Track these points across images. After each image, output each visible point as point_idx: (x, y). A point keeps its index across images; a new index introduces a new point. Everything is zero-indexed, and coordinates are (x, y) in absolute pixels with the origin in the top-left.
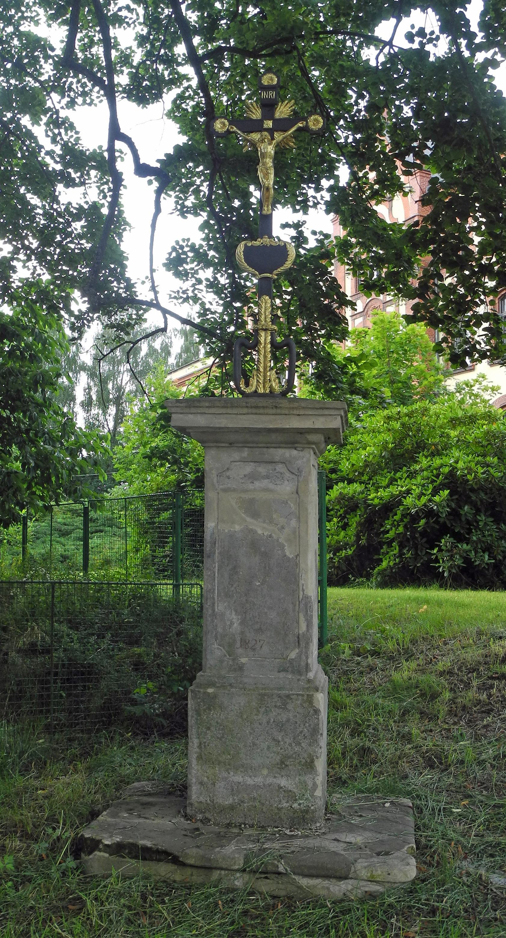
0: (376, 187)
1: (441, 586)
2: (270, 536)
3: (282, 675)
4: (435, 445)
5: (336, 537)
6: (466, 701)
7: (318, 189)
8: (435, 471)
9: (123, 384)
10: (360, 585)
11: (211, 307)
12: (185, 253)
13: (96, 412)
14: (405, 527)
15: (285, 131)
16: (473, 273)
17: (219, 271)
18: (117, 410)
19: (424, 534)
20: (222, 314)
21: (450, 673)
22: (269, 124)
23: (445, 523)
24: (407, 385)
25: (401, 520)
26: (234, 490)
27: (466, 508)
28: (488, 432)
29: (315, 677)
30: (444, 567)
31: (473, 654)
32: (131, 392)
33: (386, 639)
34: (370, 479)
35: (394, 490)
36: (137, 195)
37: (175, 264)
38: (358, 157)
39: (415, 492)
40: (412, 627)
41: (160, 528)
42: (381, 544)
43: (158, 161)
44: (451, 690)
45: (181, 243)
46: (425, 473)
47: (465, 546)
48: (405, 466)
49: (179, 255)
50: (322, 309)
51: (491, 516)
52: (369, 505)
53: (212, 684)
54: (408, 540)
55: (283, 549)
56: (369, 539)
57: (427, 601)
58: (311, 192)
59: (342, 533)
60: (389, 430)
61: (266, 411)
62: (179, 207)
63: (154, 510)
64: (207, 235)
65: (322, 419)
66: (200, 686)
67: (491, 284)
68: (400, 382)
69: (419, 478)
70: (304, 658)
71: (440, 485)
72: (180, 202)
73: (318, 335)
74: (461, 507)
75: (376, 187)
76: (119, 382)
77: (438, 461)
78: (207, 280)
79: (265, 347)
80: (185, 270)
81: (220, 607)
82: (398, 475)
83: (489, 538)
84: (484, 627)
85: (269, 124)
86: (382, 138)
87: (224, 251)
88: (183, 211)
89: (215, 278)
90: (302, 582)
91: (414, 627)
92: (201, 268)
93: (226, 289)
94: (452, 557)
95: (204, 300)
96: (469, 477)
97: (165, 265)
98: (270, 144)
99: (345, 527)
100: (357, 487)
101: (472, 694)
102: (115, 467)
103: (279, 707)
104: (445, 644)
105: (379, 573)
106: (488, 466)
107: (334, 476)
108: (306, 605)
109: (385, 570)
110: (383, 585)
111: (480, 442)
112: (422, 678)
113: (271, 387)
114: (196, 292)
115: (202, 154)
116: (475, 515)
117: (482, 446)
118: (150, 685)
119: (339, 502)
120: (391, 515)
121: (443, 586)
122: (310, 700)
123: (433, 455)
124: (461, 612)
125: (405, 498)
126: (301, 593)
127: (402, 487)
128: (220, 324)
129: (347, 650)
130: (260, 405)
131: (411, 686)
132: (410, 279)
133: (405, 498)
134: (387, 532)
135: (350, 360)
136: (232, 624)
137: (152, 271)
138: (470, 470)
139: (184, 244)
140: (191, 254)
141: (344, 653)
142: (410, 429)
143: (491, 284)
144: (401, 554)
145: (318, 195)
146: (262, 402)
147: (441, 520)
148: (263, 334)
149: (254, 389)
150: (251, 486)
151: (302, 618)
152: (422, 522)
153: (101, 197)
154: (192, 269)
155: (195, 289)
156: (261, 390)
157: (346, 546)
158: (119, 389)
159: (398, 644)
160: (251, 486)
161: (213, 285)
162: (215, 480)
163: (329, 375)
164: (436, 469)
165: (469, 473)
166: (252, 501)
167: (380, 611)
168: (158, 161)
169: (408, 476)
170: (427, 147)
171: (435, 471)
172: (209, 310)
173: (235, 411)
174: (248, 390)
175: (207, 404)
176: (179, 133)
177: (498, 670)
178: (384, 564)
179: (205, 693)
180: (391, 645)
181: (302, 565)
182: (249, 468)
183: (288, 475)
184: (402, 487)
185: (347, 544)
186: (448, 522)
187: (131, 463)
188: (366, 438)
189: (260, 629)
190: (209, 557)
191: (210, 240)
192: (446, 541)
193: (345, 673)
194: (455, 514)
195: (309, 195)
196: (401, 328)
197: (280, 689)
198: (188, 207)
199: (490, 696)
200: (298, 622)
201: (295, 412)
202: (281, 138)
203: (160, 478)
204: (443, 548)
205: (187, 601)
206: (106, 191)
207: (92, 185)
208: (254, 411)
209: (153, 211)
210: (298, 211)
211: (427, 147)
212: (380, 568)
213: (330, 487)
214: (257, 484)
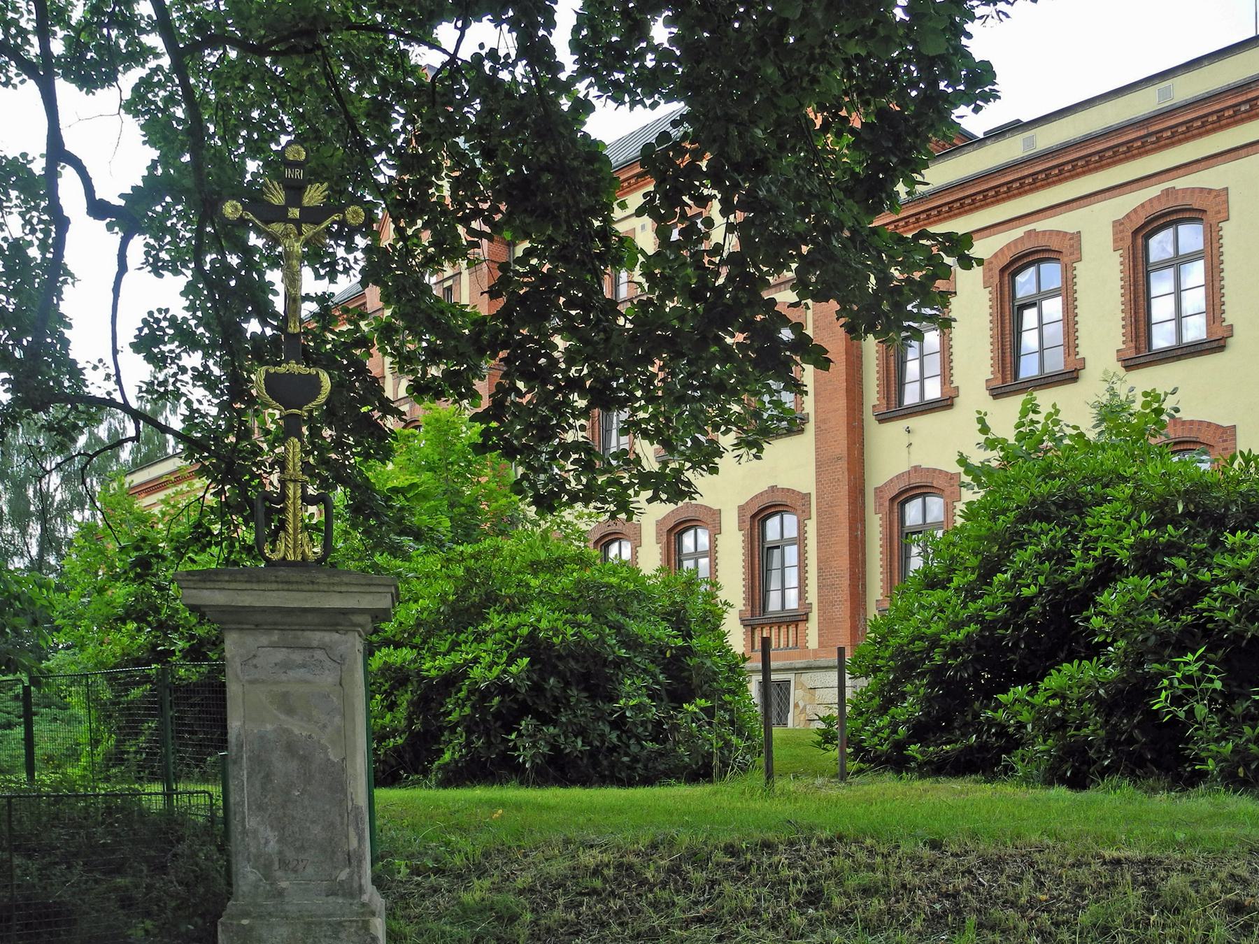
0: (431, 250)
1: (521, 783)
2: (310, 736)
3: (331, 899)
4: (511, 597)
5: (380, 721)
6: (550, 923)
7: (350, 248)
8: (510, 633)
9: (51, 490)
10: (415, 784)
11: (201, 407)
12: (162, 329)
13: (9, 531)
14: (473, 706)
15: (319, 223)
16: (559, 389)
17: (211, 356)
18: (44, 529)
19: (498, 715)
20: (216, 418)
21: (532, 890)
22: (295, 213)
23: (525, 700)
24: (472, 510)
25: (468, 698)
26: (263, 682)
27: (552, 681)
28: (579, 582)
29: (370, 900)
30: (525, 756)
31: (559, 867)
32: (63, 501)
33: (452, 853)
34: (424, 642)
35: (457, 658)
36: (90, 246)
37: (147, 344)
38: (407, 206)
39: (485, 661)
40: (483, 837)
41: (129, 709)
42: (441, 729)
43: (122, 196)
44: (533, 910)
45: (156, 315)
46: (498, 635)
47: (551, 729)
48: (471, 624)
49: (152, 330)
50: (358, 417)
51: (585, 690)
52: (424, 678)
53: (246, 915)
54: (477, 724)
55: (326, 753)
56: (425, 723)
57: (502, 804)
58: (341, 252)
59: (389, 716)
60: (449, 577)
61: (304, 587)
62: (151, 260)
63: (120, 684)
64: (192, 303)
65: (369, 598)
66: (232, 917)
67: (582, 403)
68: (463, 505)
69: (490, 642)
70: (356, 878)
71: (517, 650)
72: (153, 253)
73: (352, 453)
74: (546, 680)
75: (431, 250)
76: (45, 487)
77: (514, 620)
78: (194, 369)
79: (294, 503)
80: (162, 352)
81: (251, 823)
82: (462, 637)
83: (583, 719)
84: (573, 834)
85: (295, 213)
86: (440, 183)
87: (218, 329)
88: (157, 268)
89: (206, 367)
90: (350, 790)
91: (486, 836)
92: (185, 351)
93: (222, 383)
94: (534, 745)
95: (190, 396)
96: (554, 639)
97: (132, 345)
98: (297, 241)
99: (392, 707)
100: (406, 654)
101: (558, 914)
102: (57, 623)
103: (330, 937)
104: (526, 856)
105: (439, 768)
106: (579, 625)
107: (374, 638)
108: (356, 816)
109: (448, 764)
110: (445, 783)
111: (568, 595)
112: (497, 897)
113: (303, 553)
114: (178, 384)
115: (186, 191)
116: (564, 690)
117: (573, 599)
118: (149, 924)
119: (383, 675)
120: (453, 691)
121: (524, 783)
122: (366, 926)
123: (507, 610)
124: (545, 817)
125: (472, 668)
126: (350, 803)
127: (467, 654)
128: (215, 431)
129: (403, 869)
130: (294, 579)
131: (484, 908)
132: (476, 381)
133: (472, 668)
134: (450, 714)
135: (395, 490)
136: (267, 842)
137: (115, 352)
138: (556, 632)
139: (161, 317)
140: (171, 332)
141: (399, 872)
142: (477, 576)
143: (582, 403)
144: (469, 744)
145: (351, 257)
146: (293, 575)
147: (520, 697)
148: (291, 486)
149: (281, 555)
150: (284, 677)
151: (352, 833)
152: (497, 700)
153: (27, 231)
154: (172, 351)
155: (177, 380)
156: (291, 557)
157: (394, 733)
158: (44, 496)
159: (467, 859)
160: (284, 677)
161: (201, 376)
162: (239, 672)
163: (366, 504)
164: (512, 630)
165: (554, 635)
166: (285, 695)
167: (442, 818)
168: (122, 196)
169: (475, 639)
170: (499, 211)
171: (510, 633)
172: (198, 411)
173: (262, 586)
174: (274, 557)
175: (227, 578)
176: (144, 143)
177: (589, 884)
178: (447, 757)
179: (238, 925)
180: (458, 861)
181: (350, 771)
182: (281, 655)
183: (328, 663)
184: (467, 654)
185: (395, 730)
186: (528, 699)
187: (81, 616)
188: (417, 586)
189: (302, 847)
190: (235, 762)
191: (197, 310)
192: (526, 724)
193: (402, 897)
194: (537, 689)
195: (339, 256)
196: (464, 429)
197: (329, 915)
198: (163, 261)
199: (578, 915)
200: (347, 837)
201: (336, 588)
202: (311, 233)
203: (126, 640)
204: (524, 732)
205: (185, 813)
206: (35, 221)
207: (13, 210)
208: (286, 587)
209: (116, 269)
210: (322, 277)
211: (499, 211)
212: (441, 762)
213: (372, 654)
214: (291, 674)
